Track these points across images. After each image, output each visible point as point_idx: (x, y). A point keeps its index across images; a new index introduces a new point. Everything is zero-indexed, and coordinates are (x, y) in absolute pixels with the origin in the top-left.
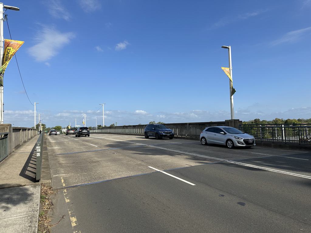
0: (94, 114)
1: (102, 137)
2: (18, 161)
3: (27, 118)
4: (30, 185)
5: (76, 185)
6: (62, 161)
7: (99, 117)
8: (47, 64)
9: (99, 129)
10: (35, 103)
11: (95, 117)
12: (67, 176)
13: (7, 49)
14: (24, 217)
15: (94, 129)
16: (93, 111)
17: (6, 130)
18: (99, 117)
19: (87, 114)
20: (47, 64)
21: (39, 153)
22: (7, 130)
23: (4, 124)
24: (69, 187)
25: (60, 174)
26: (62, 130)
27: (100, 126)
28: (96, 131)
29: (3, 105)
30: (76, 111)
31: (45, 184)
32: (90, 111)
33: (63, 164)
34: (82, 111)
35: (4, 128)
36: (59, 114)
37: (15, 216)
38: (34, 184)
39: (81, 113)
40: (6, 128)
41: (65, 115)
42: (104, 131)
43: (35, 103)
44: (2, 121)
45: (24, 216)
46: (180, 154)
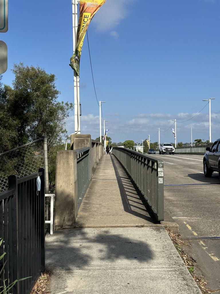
0: (190, 119)
1: (199, 159)
2: (108, 191)
3: (86, 127)
4: (150, 226)
5: (215, 236)
6: (169, 196)
7: (198, 124)
8: (114, 34)
9: (197, 146)
10: (100, 102)
11: (192, 126)
12: (192, 221)
13: (83, 16)
14: (171, 271)
15: (186, 146)
16: (187, 114)
17: (86, 143)
18: (198, 124)
19: (178, 119)
20: (114, 34)
21: (162, 183)
22: (87, 144)
23: (82, 134)
24: (207, 238)
25: (179, 217)
26: (135, 148)
27: (199, 141)
28: (194, 150)
29: (79, 105)
30: (159, 115)
31: (170, 227)
32: (182, 115)
33: (174, 201)
34: (169, 115)
35: (83, 141)
36: (133, 120)
37: (155, 267)
38: (155, 226)
39: (167, 118)
40: (86, 141)
41: (143, 121)
42: (183, 150)
43: (100, 102)
44: (79, 130)
45: (169, 269)
46: (76, 185)
